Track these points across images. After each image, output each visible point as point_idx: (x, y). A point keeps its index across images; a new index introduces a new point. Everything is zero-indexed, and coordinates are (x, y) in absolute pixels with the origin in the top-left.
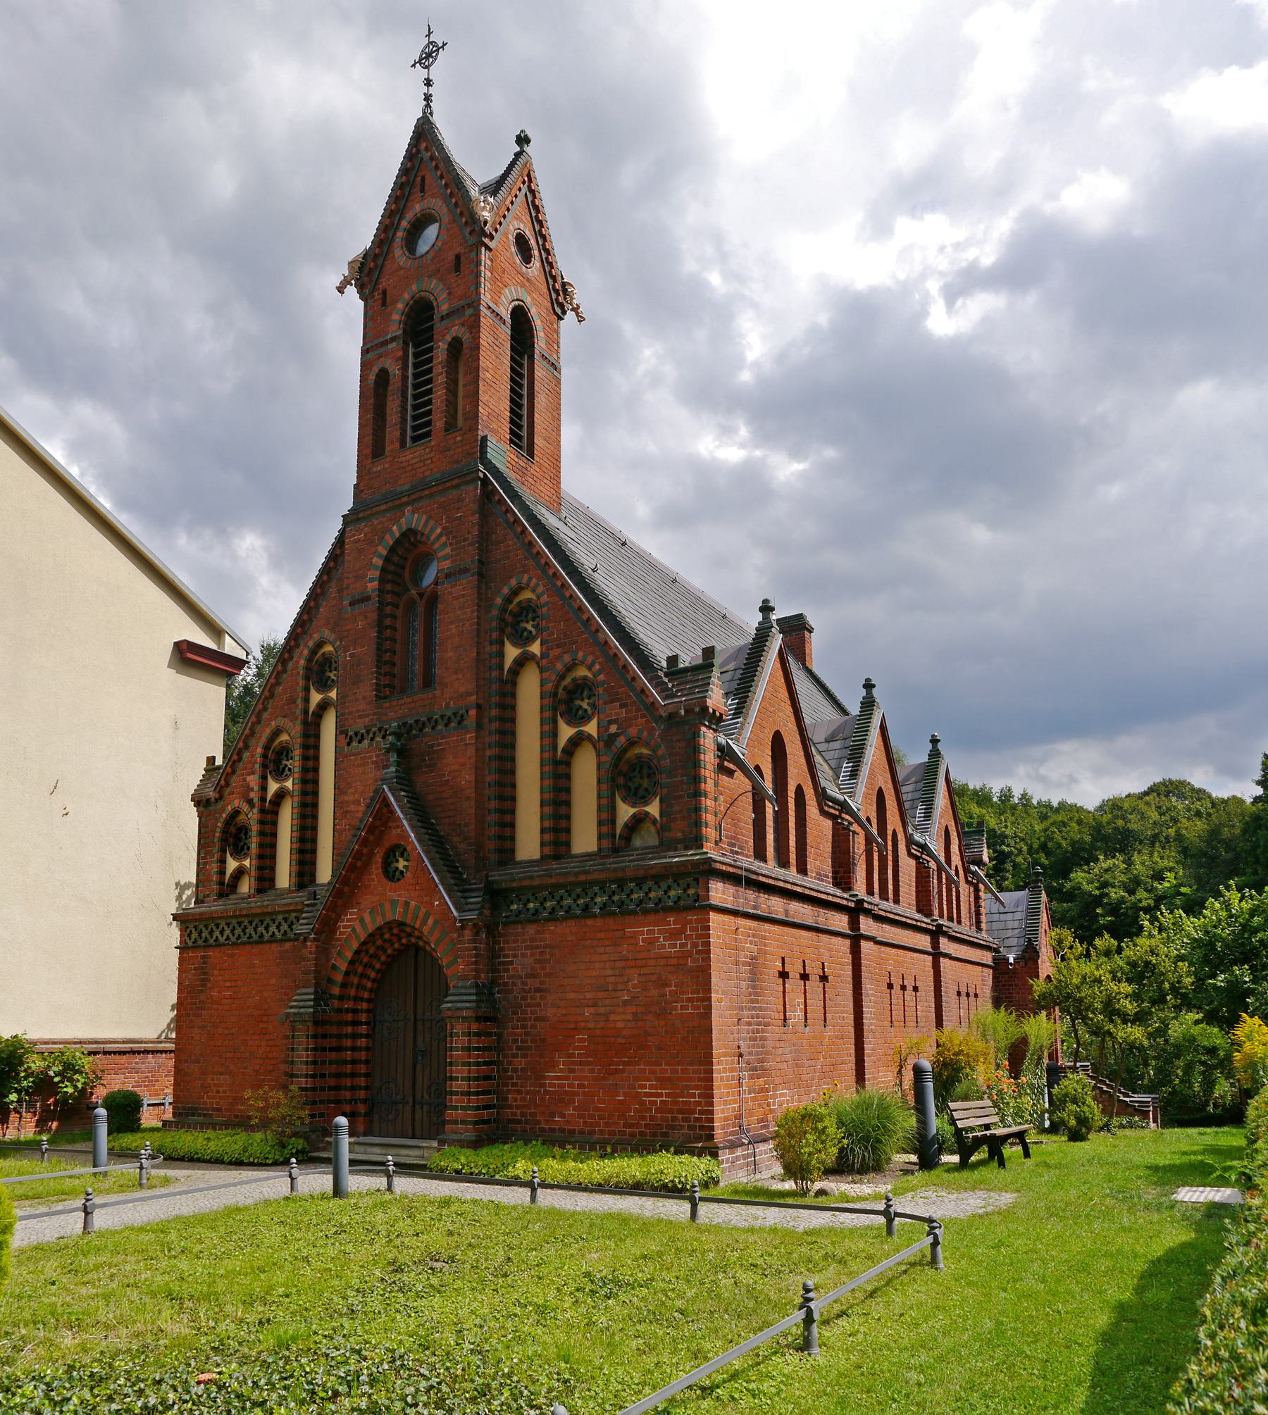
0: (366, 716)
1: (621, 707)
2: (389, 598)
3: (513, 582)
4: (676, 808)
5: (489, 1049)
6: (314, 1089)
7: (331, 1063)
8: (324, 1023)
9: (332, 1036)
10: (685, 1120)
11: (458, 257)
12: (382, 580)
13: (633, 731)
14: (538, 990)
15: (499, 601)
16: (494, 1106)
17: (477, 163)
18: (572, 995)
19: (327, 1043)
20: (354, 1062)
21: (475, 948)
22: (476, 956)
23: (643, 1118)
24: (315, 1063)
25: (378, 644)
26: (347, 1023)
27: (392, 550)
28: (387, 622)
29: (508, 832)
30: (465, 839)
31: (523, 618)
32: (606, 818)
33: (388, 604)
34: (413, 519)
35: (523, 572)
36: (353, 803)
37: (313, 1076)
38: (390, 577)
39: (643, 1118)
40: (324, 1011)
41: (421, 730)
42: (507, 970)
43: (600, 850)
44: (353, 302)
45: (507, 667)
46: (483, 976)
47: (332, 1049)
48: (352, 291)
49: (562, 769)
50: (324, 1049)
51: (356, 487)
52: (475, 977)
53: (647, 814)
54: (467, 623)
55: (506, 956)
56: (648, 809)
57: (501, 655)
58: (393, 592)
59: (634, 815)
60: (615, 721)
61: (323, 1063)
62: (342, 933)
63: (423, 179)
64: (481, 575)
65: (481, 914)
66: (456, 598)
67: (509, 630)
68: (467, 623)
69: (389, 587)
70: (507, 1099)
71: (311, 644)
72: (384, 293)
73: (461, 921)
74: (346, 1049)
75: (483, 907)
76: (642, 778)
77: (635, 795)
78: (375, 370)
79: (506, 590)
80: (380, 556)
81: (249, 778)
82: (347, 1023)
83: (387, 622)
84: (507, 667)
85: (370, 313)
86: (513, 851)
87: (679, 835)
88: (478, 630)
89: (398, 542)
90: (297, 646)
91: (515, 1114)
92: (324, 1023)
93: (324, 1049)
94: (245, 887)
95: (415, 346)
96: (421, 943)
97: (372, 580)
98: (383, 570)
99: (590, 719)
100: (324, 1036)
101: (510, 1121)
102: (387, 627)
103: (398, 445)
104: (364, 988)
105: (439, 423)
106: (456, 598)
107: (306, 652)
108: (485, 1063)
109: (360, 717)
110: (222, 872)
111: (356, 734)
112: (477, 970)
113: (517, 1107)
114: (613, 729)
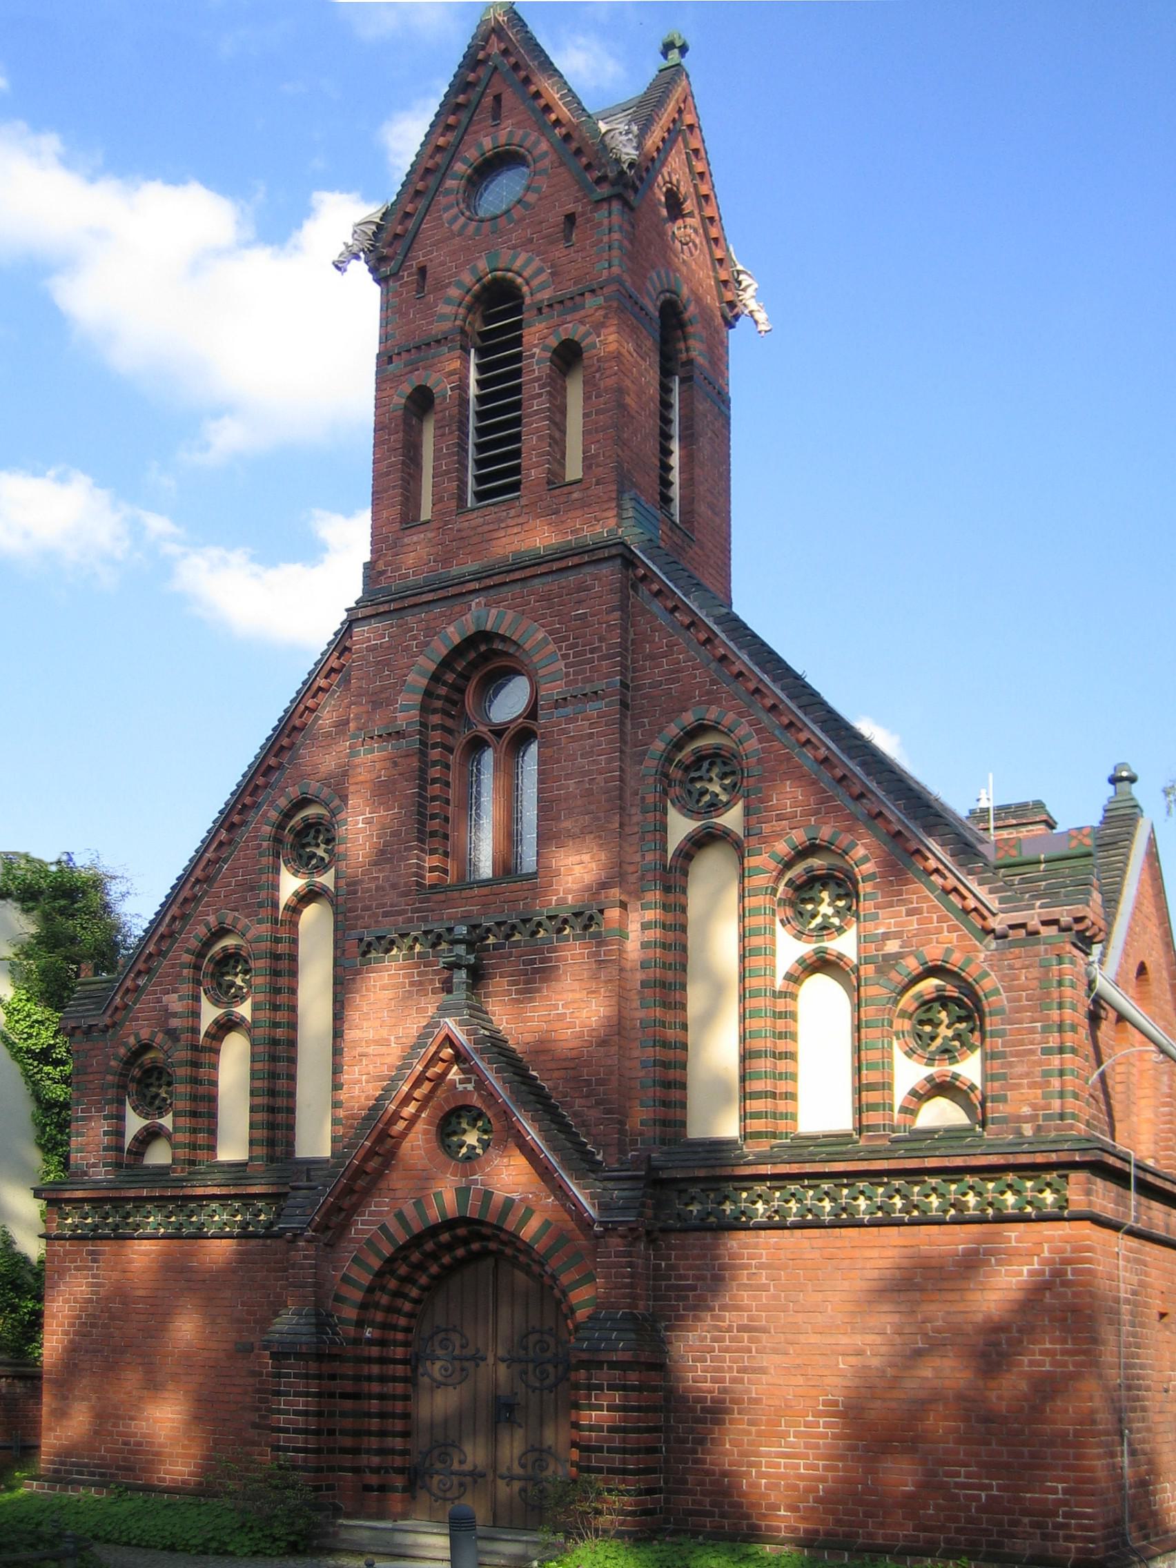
0: (400, 913)
1: (910, 913)
2: (436, 736)
3: (689, 718)
4: (1020, 1069)
5: (654, 1409)
6: (318, 1451)
7: (343, 1414)
8: (334, 1357)
9: (343, 1377)
10: (1035, 1525)
11: (570, 219)
12: (425, 709)
13: (933, 953)
14: (742, 1329)
15: (659, 746)
16: (660, 1491)
17: (594, 72)
18: (814, 1339)
19: (338, 1386)
20: (382, 1415)
21: (630, 1265)
22: (632, 1276)
23: (956, 1519)
24: (319, 1414)
25: (420, 805)
26: (369, 1360)
27: (446, 663)
28: (435, 772)
29: (675, 1094)
30: (598, 1103)
31: (309, 839)
32: (867, 1086)
33: (435, 746)
34: (481, 614)
35: (710, 703)
36: (377, 1042)
37: (317, 1432)
38: (439, 704)
39: (956, 1519)
40: (333, 1342)
41: (508, 937)
42: (686, 1298)
43: (251, 1158)
44: (363, 294)
45: (672, 848)
46: (641, 1303)
47: (344, 1396)
48: (359, 270)
49: (781, 1004)
50: (332, 1395)
51: (368, 567)
52: (629, 1306)
53: (955, 1076)
54: (600, 779)
55: (681, 1277)
56: (160, 1121)
57: (662, 828)
58: (444, 728)
59: (146, 1128)
60: (897, 935)
61: (332, 1414)
62: (358, 1232)
63: (498, 99)
64: (624, 705)
65: (640, 1215)
66: (573, 739)
67: (676, 790)
68: (600, 779)
69: (435, 719)
70: (685, 1482)
71: (283, 802)
72: (422, 271)
73: (601, 1223)
74: (370, 1396)
75: (643, 1205)
76: (160, 1086)
77: (151, 1104)
78: (407, 389)
79: (673, 730)
80: (421, 673)
81: (165, 998)
82: (369, 1360)
83: (435, 772)
84: (672, 848)
85: (395, 301)
86: (683, 1124)
87: (1026, 1110)
88: (621, 789)
89: (458, 651)
90: (255, 805)
91: (700, 1503)
92: (334, 1357)
93: (332, 1395)
94: (159, 1155)
95: (481, 353)
96: (509, 1251)
97: (405, 708)
98: (428, 694)
99: (243, 999)
100: (333, 1377)
101: (690, 1513)
102: (434, 781)
103: (453, 504)
104: (398, 1311)
105: (533, 472)
106: (573, 739)
107: (274, 815)
108: (649, 1430)
109: (386, 914)
110: (119, 1133)
111: (379, 938)
112: (634, 1297)
113: (704, 1493)
114: (892, 946)
